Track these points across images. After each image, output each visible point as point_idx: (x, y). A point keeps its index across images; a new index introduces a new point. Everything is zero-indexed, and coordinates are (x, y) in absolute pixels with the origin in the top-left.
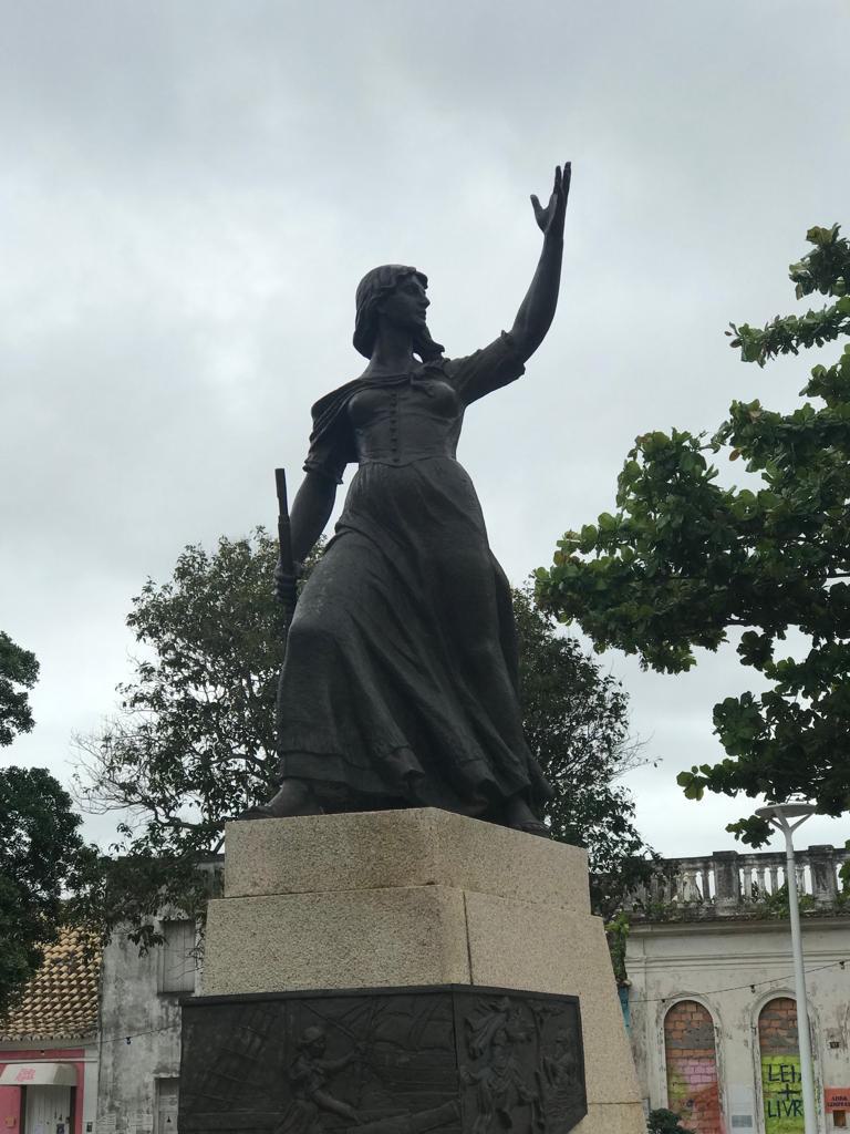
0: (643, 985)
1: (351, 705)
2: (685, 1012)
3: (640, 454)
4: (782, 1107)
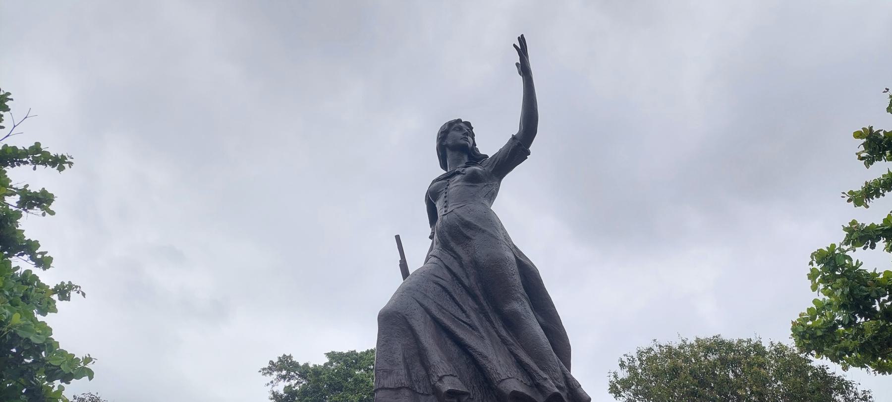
3: (814, 262)
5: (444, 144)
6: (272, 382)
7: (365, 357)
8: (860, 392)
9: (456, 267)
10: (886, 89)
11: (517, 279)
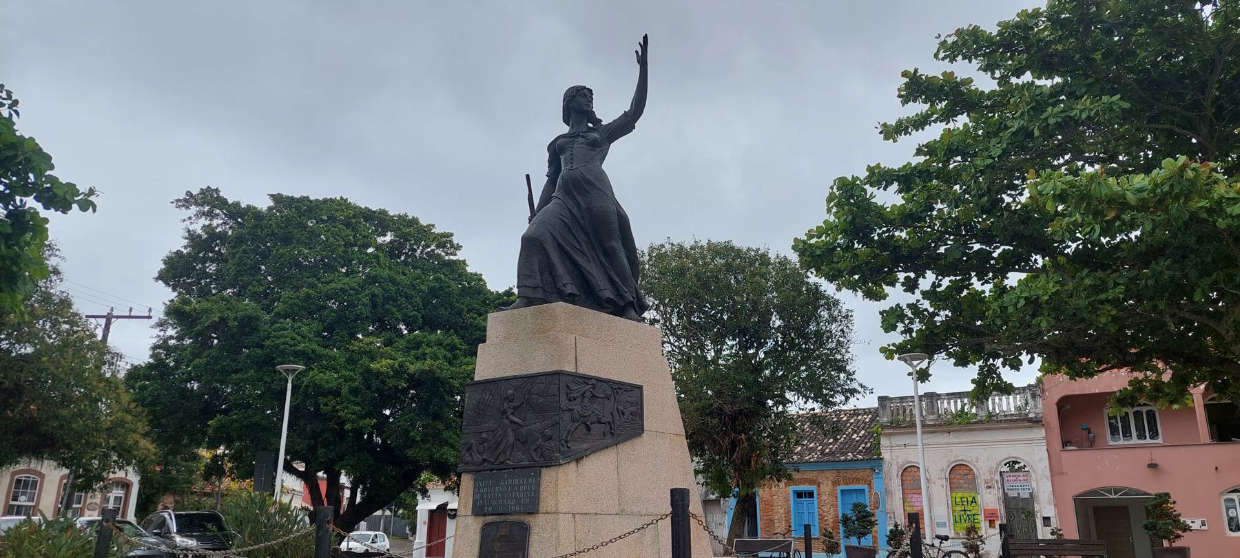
0: (890, 458)
1: (548, 267)
2: (911, 471)
3: (835, 187)
4: (962, 517)
5: (571, 105)
6: (190, 218)
7: (322, 206)
8: (844, 310)
9: (575, 210)
10: (939, 35)
11: (616, 226)
